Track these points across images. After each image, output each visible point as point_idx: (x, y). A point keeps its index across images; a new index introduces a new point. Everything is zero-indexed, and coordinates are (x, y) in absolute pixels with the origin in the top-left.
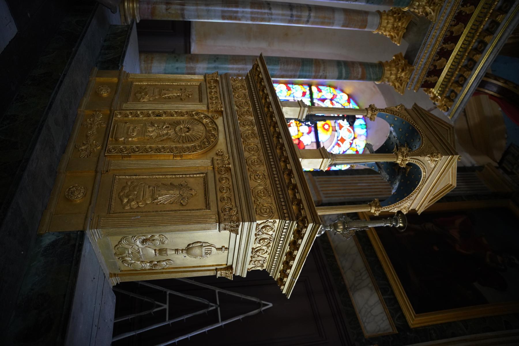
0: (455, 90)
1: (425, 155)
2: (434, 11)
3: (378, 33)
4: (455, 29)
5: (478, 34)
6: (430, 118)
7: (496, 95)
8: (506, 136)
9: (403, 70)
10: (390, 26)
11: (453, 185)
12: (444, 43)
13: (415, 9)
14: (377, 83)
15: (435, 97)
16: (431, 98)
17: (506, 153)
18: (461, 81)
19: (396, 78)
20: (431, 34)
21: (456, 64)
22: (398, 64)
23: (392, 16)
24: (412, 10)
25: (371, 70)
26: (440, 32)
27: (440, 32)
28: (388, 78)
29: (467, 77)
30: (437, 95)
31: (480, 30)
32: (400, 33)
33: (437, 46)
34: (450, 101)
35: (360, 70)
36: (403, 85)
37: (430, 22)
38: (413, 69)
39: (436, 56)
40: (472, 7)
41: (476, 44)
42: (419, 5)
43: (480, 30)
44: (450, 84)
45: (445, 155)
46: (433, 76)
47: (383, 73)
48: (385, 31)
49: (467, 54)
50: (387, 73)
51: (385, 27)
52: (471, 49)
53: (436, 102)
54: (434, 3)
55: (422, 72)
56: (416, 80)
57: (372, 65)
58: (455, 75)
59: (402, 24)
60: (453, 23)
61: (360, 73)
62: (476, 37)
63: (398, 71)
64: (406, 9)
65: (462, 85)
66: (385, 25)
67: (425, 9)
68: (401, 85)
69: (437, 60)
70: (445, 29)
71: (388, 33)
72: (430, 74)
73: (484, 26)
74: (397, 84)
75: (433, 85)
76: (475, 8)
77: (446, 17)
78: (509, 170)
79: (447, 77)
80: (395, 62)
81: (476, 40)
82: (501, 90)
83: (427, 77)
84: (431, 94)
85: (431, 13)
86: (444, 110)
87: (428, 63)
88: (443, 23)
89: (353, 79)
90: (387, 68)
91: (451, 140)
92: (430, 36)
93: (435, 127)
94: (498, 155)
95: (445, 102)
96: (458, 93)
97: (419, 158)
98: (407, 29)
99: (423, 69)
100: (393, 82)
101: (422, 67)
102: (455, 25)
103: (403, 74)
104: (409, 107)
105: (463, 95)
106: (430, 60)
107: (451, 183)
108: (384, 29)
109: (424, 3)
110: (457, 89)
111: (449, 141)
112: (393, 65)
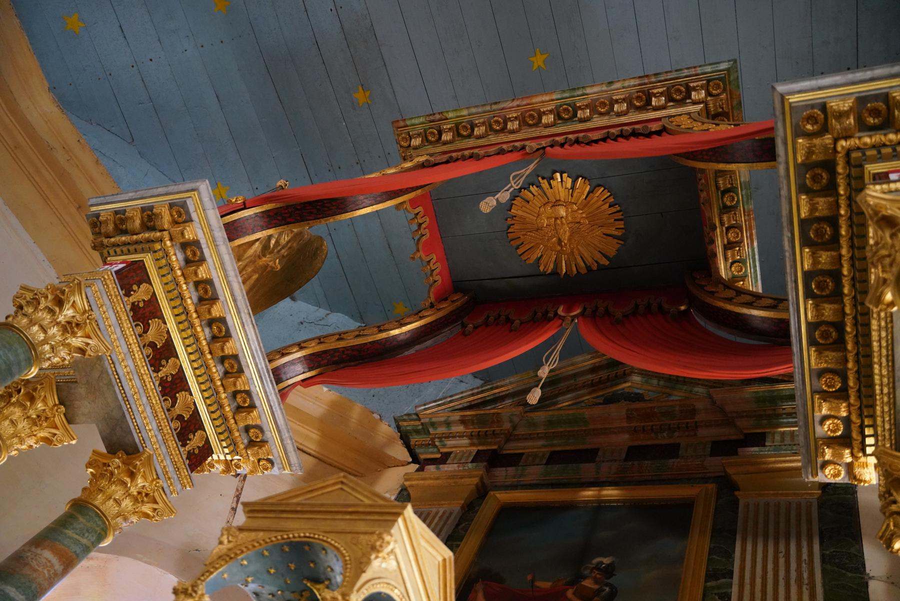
0: (251, 423)
1: (369, 562)
2: (89, 337)
3: (10, 458)
4: (151, 336)
5: (195, 315)
6: (295, 501)
7: (308, 375)
8: (377, 416)
9: (132, 475)
10: (23, 425)
11: (447, 557)
12: (157, 371)
13: (49, 359)
14: (105, 544)
15: (228, 464)
16: (223, 472)
17: (405, 438)
18: (244, 403)
19: (136, 500)
20: (121, 374)
21: (208, 384)
22: (112, 474)
23: (9, 403)
24: (46, 365)
25: (69, 533)
26: (134, 360)
27: (134, 360)
28: (119, 515)
29: (247, 388)
30: (229, 457)
31: (192, 308)
32: (57, 419)
33: (150, 386)
34: (260, 447)
35: (47, 554)
36: (158, 499)
37: (99, 358)
38: (150, 457)
39: (166, 400)
40: (144, 286)
41: (207, 330)
42: (52, 348)
43: (192, 308)
44: (232, 421)
45: (391, 527)
46: (191, 436)
47: (101, 516)
48: (22, 441)
49: (209, 356)
50: (110, 508)
51: (15, 435)
52: (208, 344)
53: (239, 471)
54: (78, 325)
55: (168, 447)
56: (170, 469)
57: (63, 522)
58: (226, 402)
59: (44, 401)
60: (139, 330)
61: (55, 561)
62: (197, 322)
63: (124, 484)
64: (34, 371)
65: (252, 406)
66: (11, 431)
67: (69, 345)
68: (156, 502)
69: (173, 406)
70: (135, 348)
71: (31, 441)
72: (183, 437)
73: (190, 298)
74: (147, 508)
75: (207, 450)
76: (151, 284)
77: (118, 330)
78: (439, 456)
79: (215, 416)
80: (102, 476)
81: (201, 325)
82: (312, 361)
83: (184, 445)
84: (217, 465)
85: (87, 344)
86: (267, 469)
87: (164, 423)
88: (123, 342)
89: (51, 585)
90: (99, 499)
91: (366, 496)
92: (123, 379)
93: (322, 505)
94: (400, 452)
95: (254, 455)
96: (259, 422)
97: (364, 577)
98: (62, 403)
99: (165, 442)
100: (135, 513)
101: (160, 437)
102: (146, 331)
103: (140, 481)
104: (241, 518)
105: (270, 418)
106: (161, 415)
107: (440, 559)
108: (15, 440)
109: (59, 338)
110: (252, 419)
111: (367, 501)
112: (104, 483)
